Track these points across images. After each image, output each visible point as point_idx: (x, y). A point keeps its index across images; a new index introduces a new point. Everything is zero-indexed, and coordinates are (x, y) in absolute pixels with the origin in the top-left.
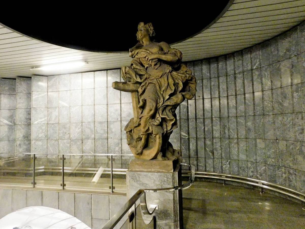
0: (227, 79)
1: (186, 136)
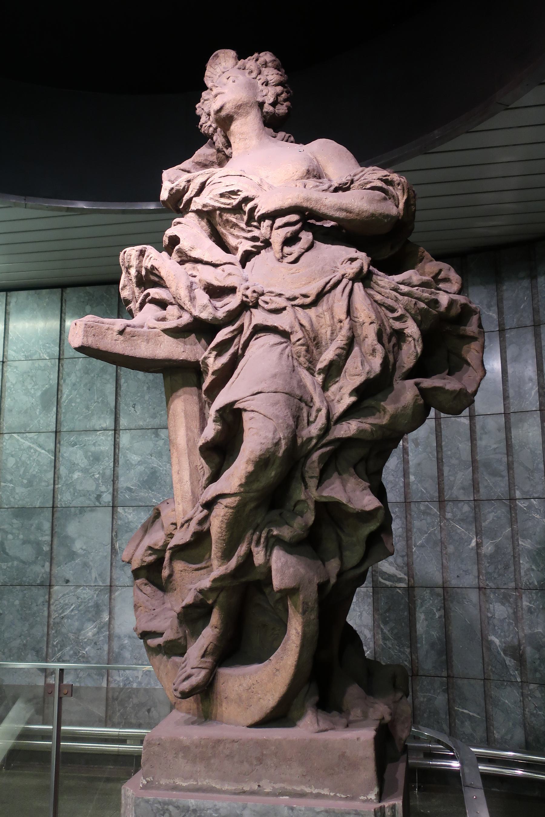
1: (400, 580)
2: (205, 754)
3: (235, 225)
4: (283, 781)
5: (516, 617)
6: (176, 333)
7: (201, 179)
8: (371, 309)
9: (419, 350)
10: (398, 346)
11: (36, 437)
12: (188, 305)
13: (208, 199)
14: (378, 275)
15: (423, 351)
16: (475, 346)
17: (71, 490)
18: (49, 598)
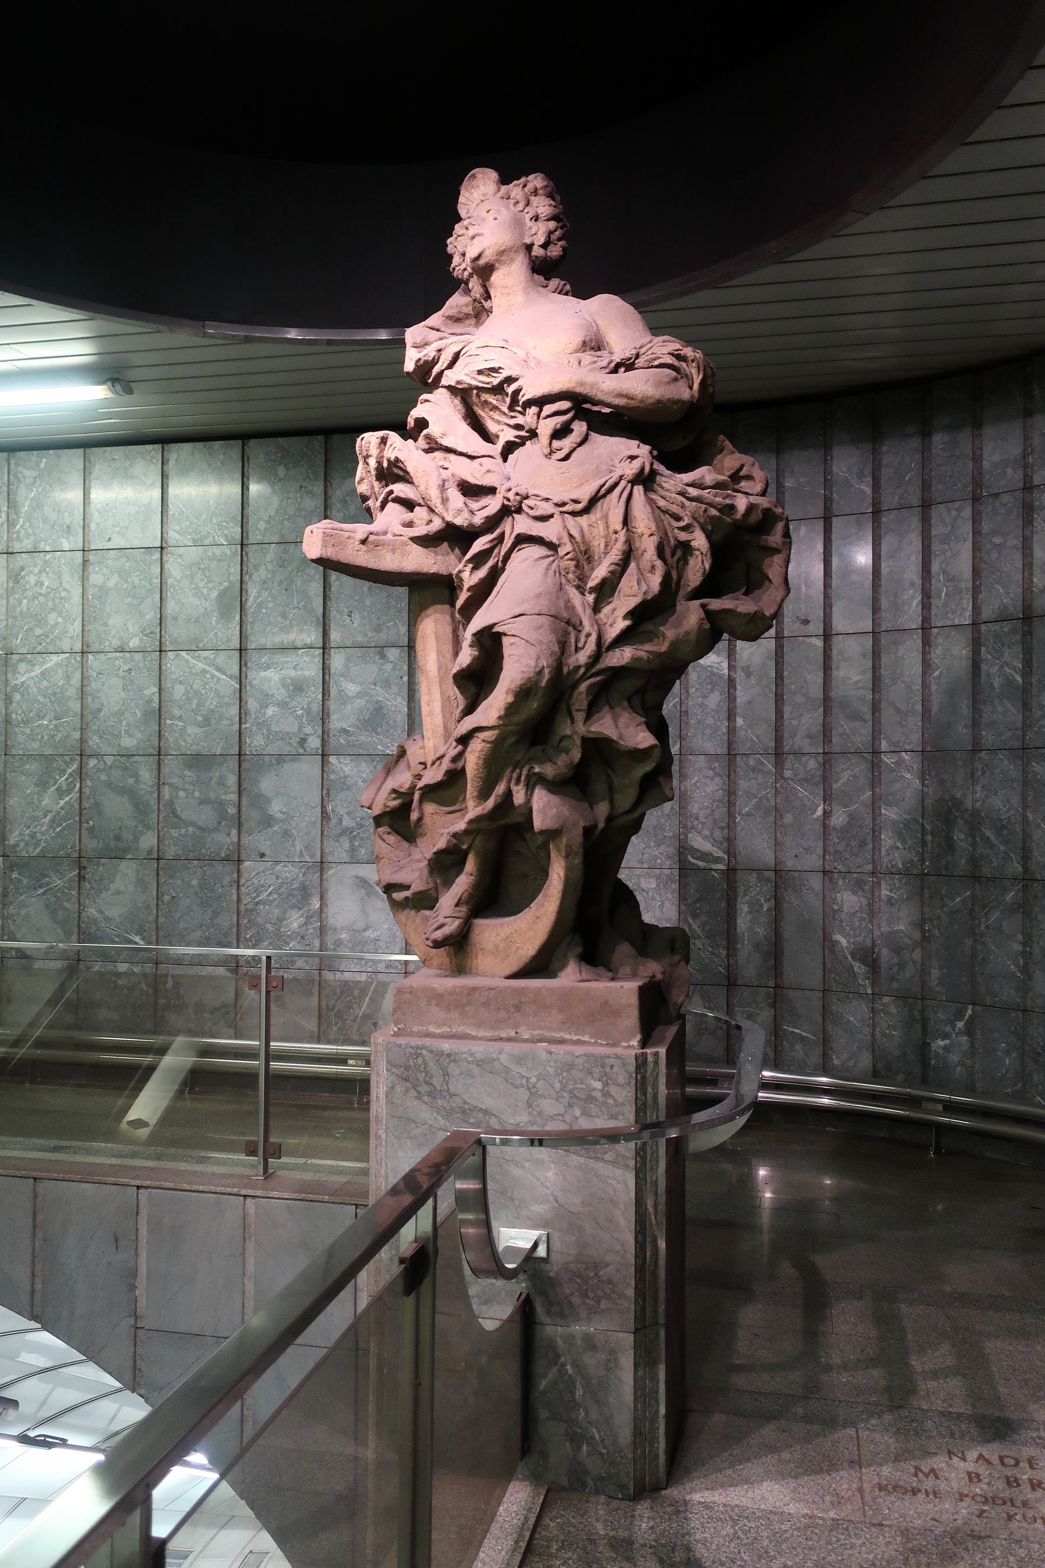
0: (976, 518)
1: (717, 860)
2: (458, 1003)
3: (495, 408)
4: (541, 1028)
5: (872, 911)
6: (427, 541)
7: (455, 349)
8: (651, 519)
9: (707, 566)
10: (684, 560)
11: (212, 657)
12: (439, 508)
13: (461, 374)
14: (662, 475)
15: (712, 567)
16: (778, 559)
17: (264, 731)
18: (238, 877)
